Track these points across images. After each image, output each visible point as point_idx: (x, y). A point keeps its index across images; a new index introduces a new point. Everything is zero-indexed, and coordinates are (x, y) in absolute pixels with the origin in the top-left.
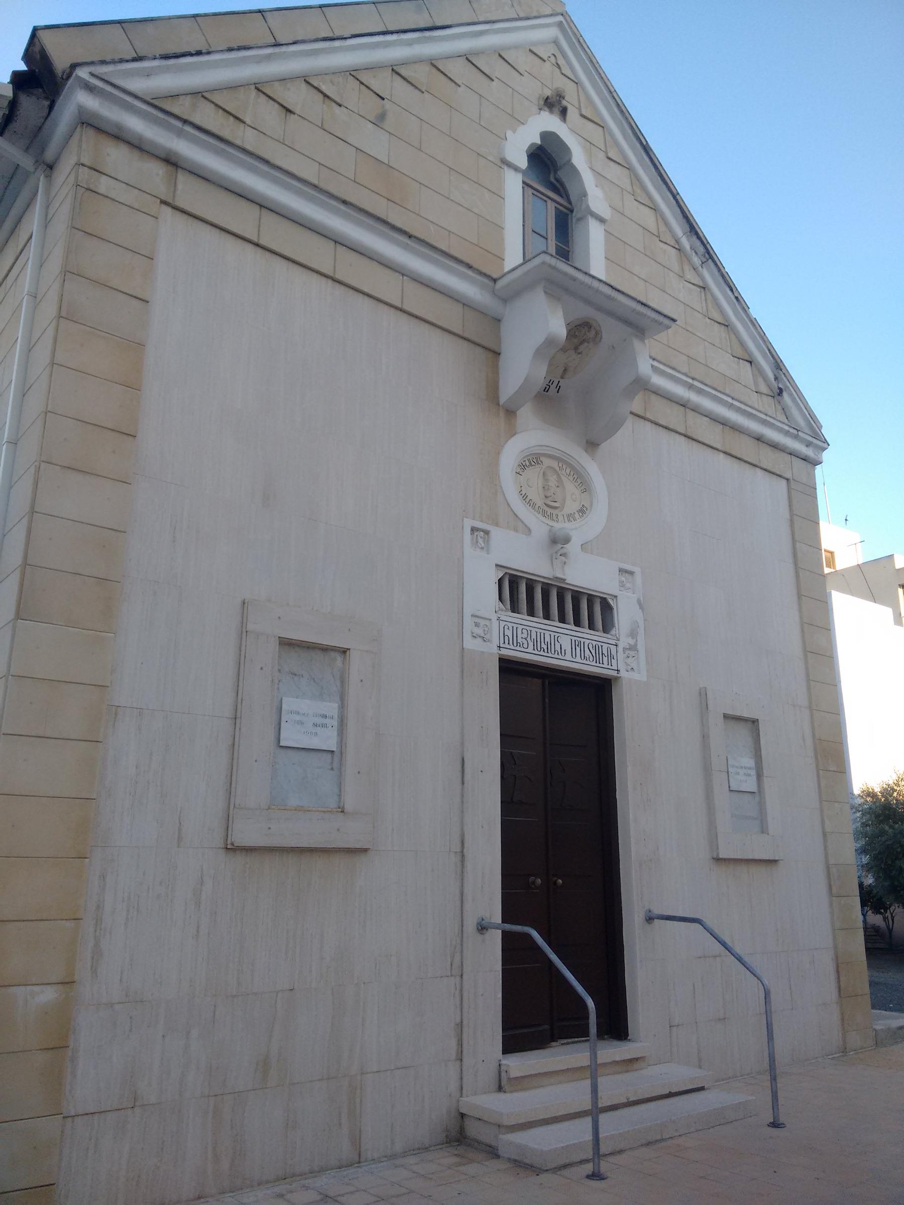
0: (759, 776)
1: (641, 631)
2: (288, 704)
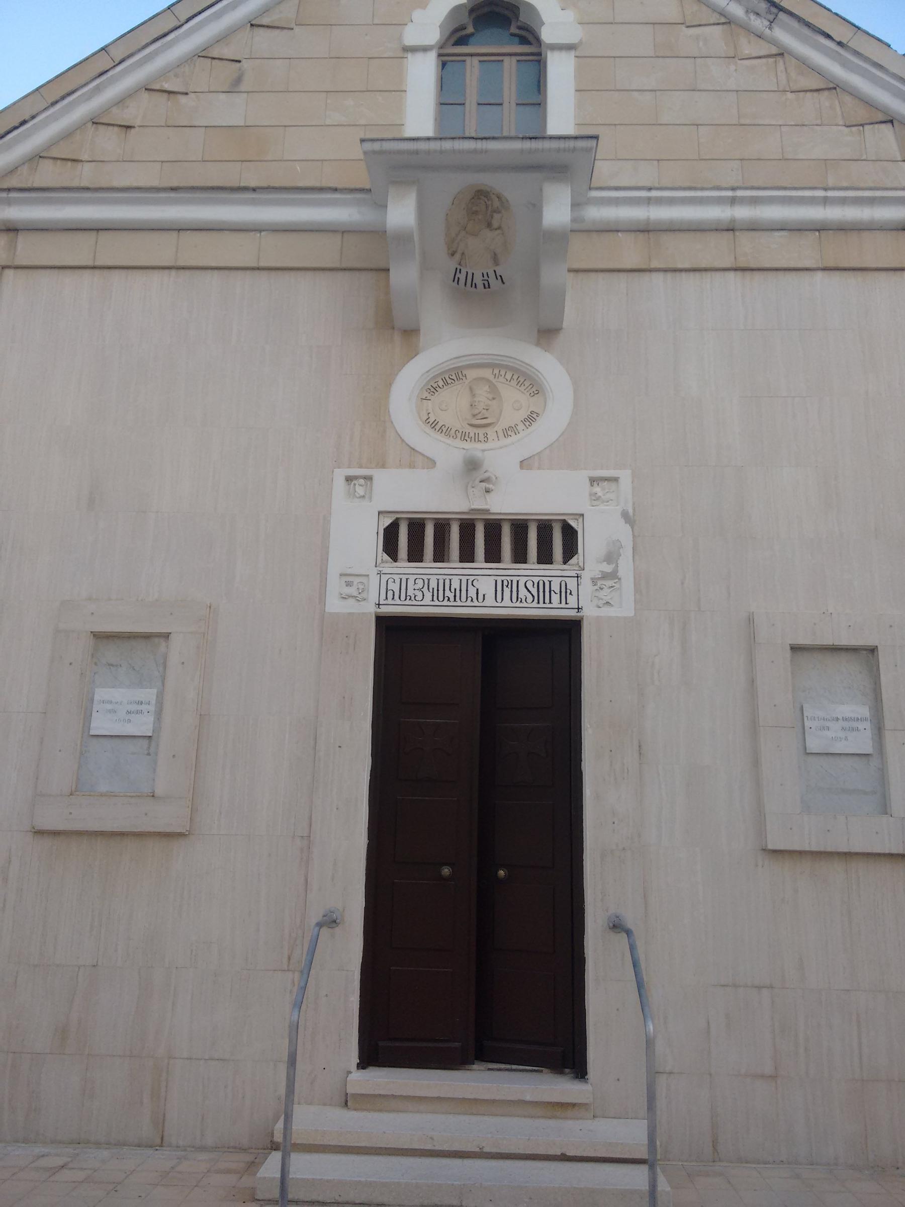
0: (879, 730)
1: (627, 552)
2: (101, 694)
